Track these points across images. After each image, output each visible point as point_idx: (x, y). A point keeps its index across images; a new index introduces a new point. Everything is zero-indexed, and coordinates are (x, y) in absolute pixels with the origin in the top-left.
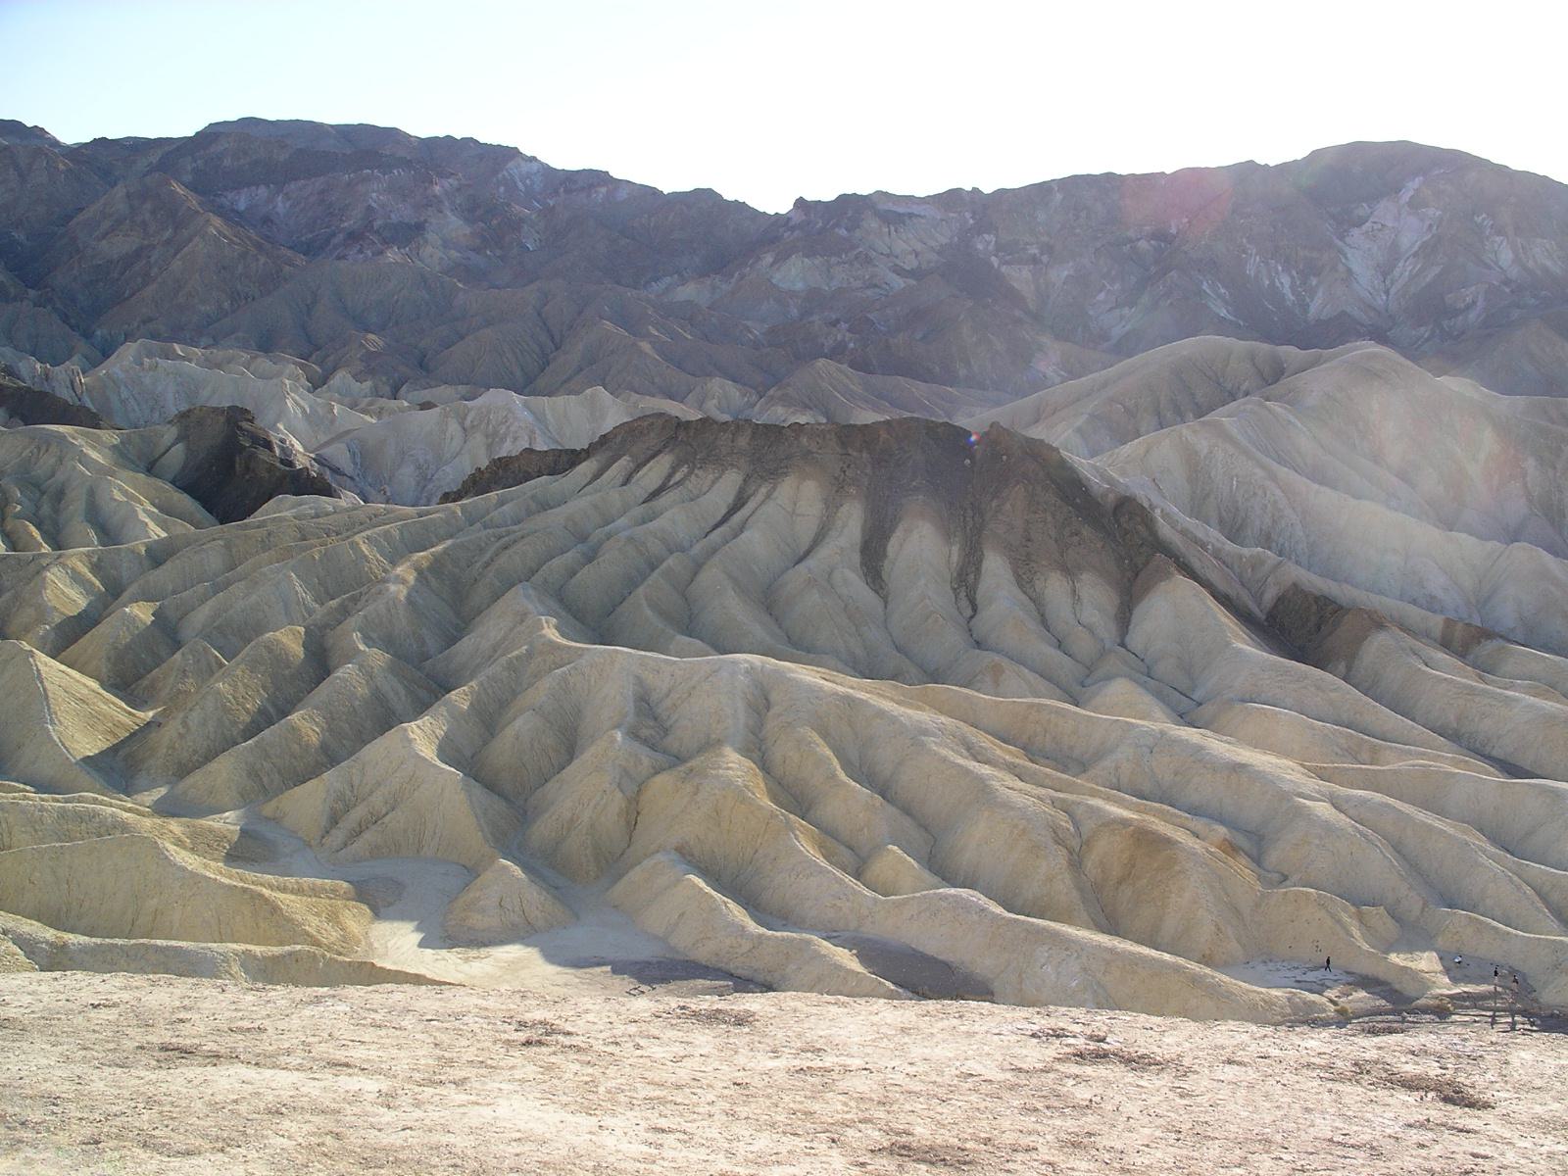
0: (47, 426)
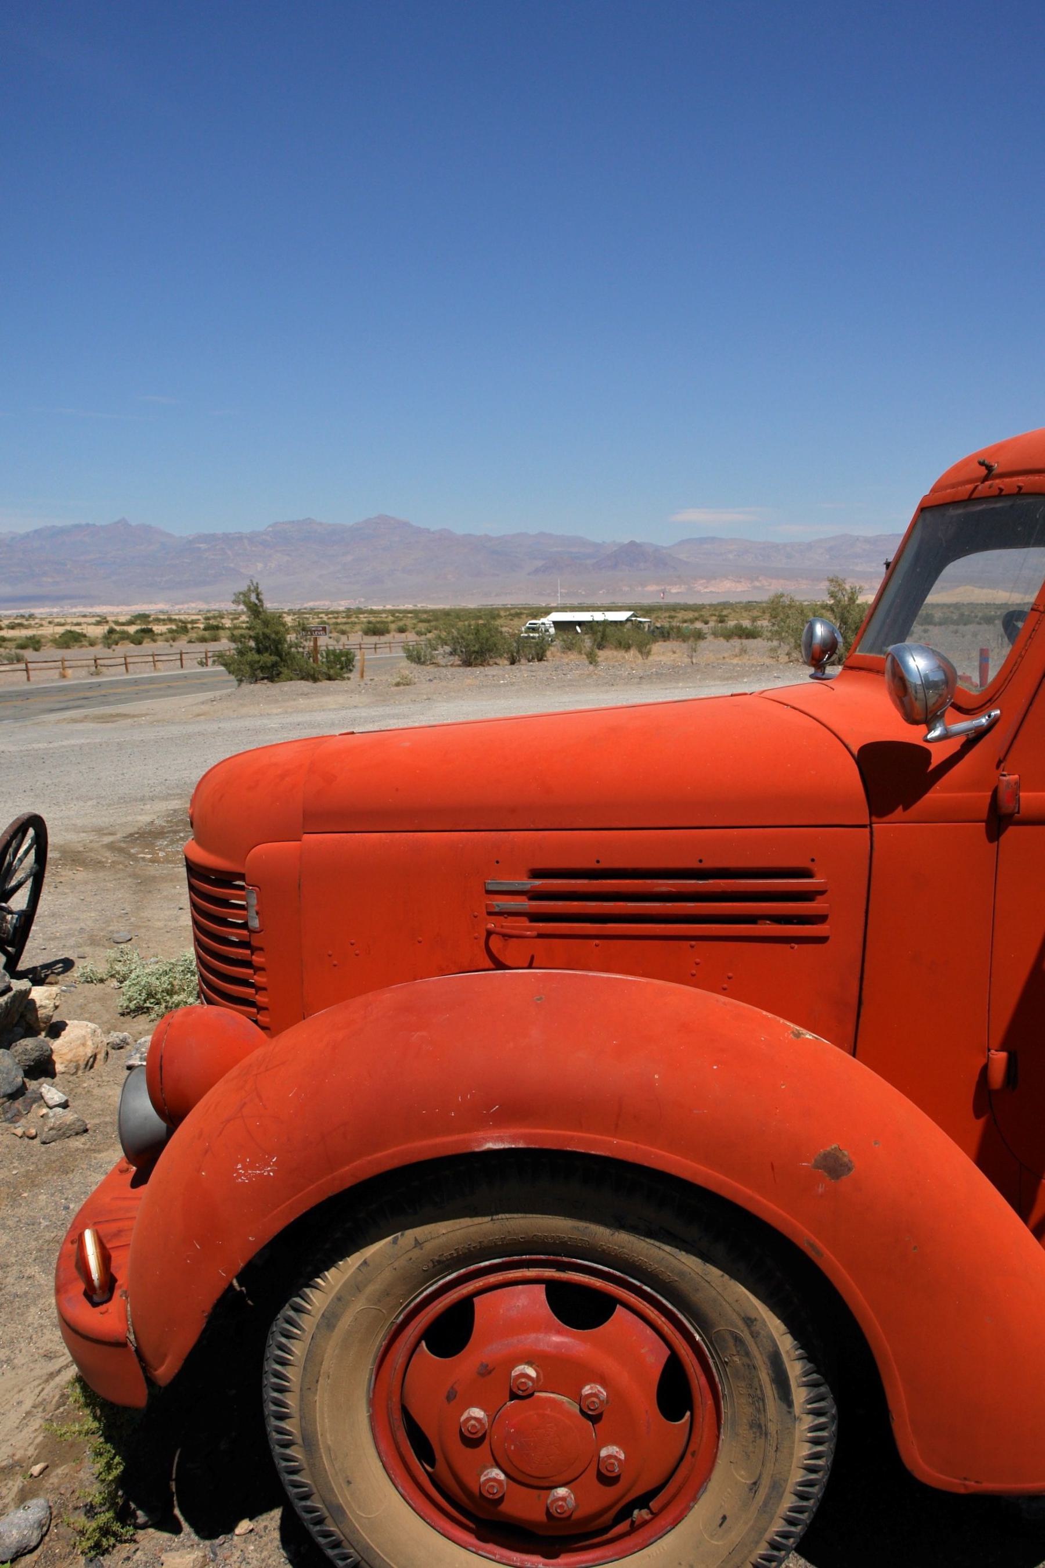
0: (3, 869)
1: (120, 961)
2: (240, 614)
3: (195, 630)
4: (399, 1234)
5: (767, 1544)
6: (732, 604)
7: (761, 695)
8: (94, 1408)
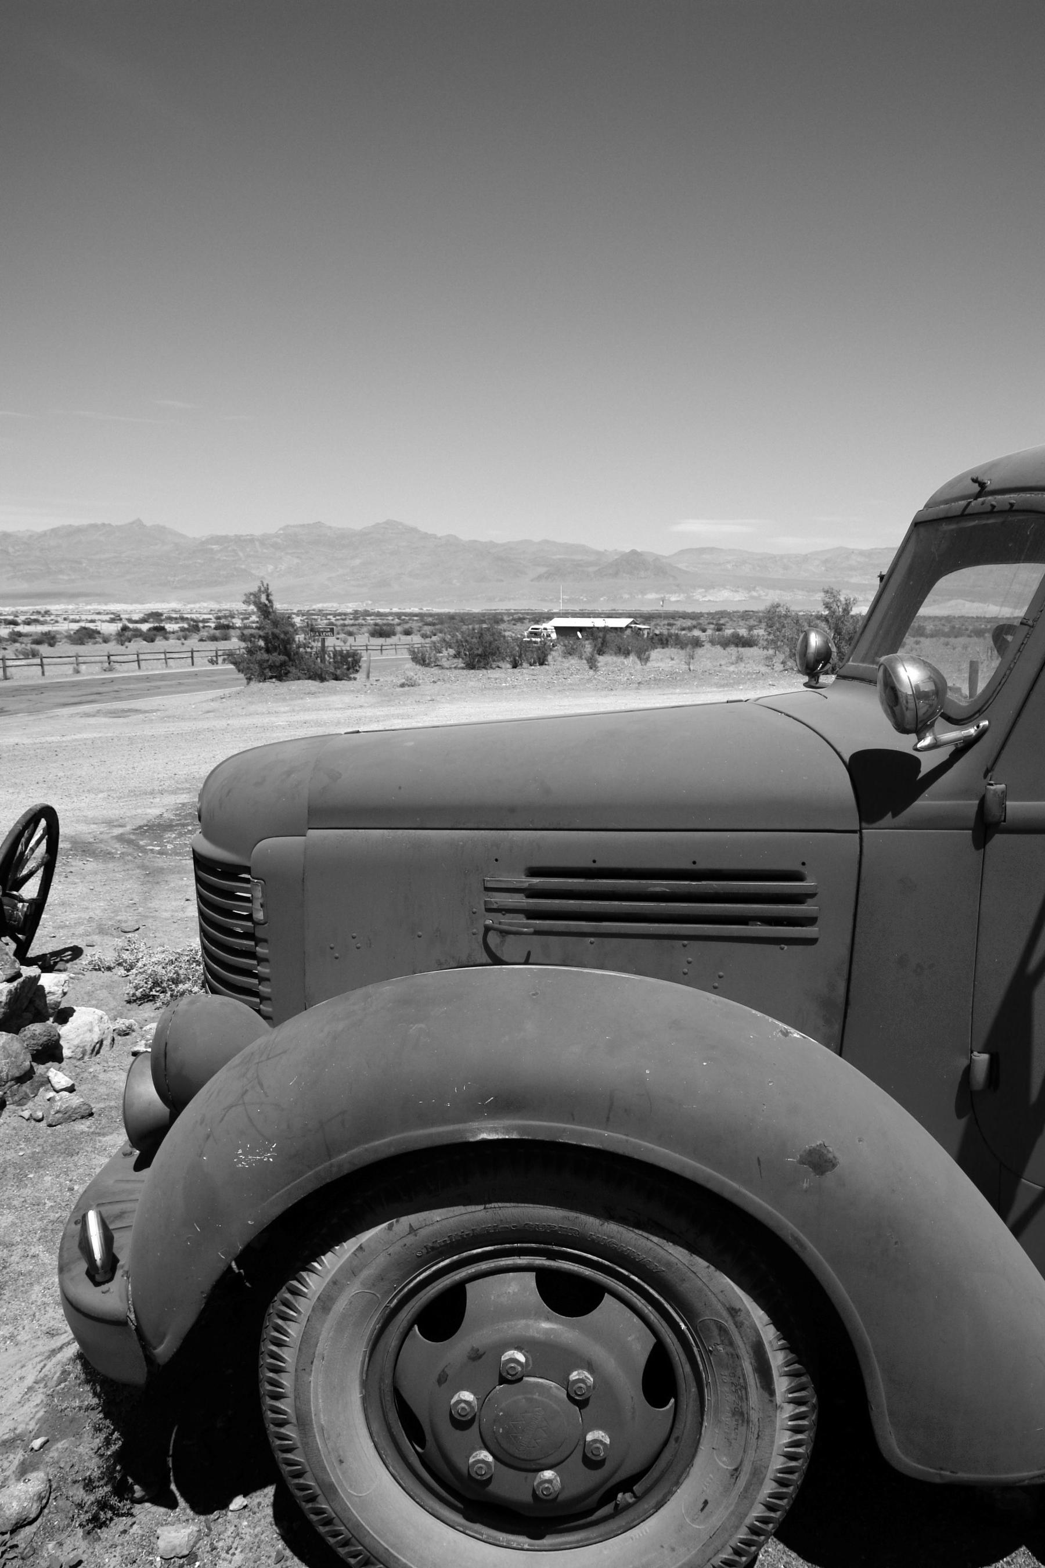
0: (16, 858)
1: (127, 950)
2: (250, 614)
3: (207, 629)
4: (395, 1220)
5: (747, 1529)
6: (729, 613)
7: (757, 702)
8: (94, 1384)
